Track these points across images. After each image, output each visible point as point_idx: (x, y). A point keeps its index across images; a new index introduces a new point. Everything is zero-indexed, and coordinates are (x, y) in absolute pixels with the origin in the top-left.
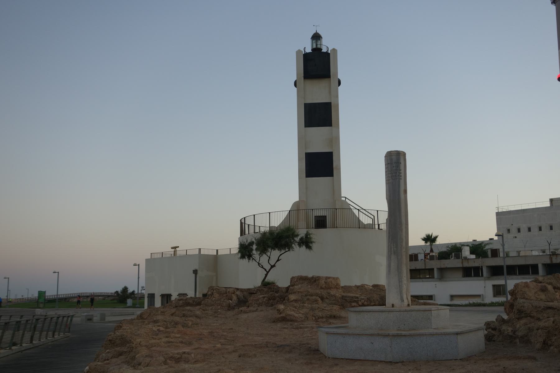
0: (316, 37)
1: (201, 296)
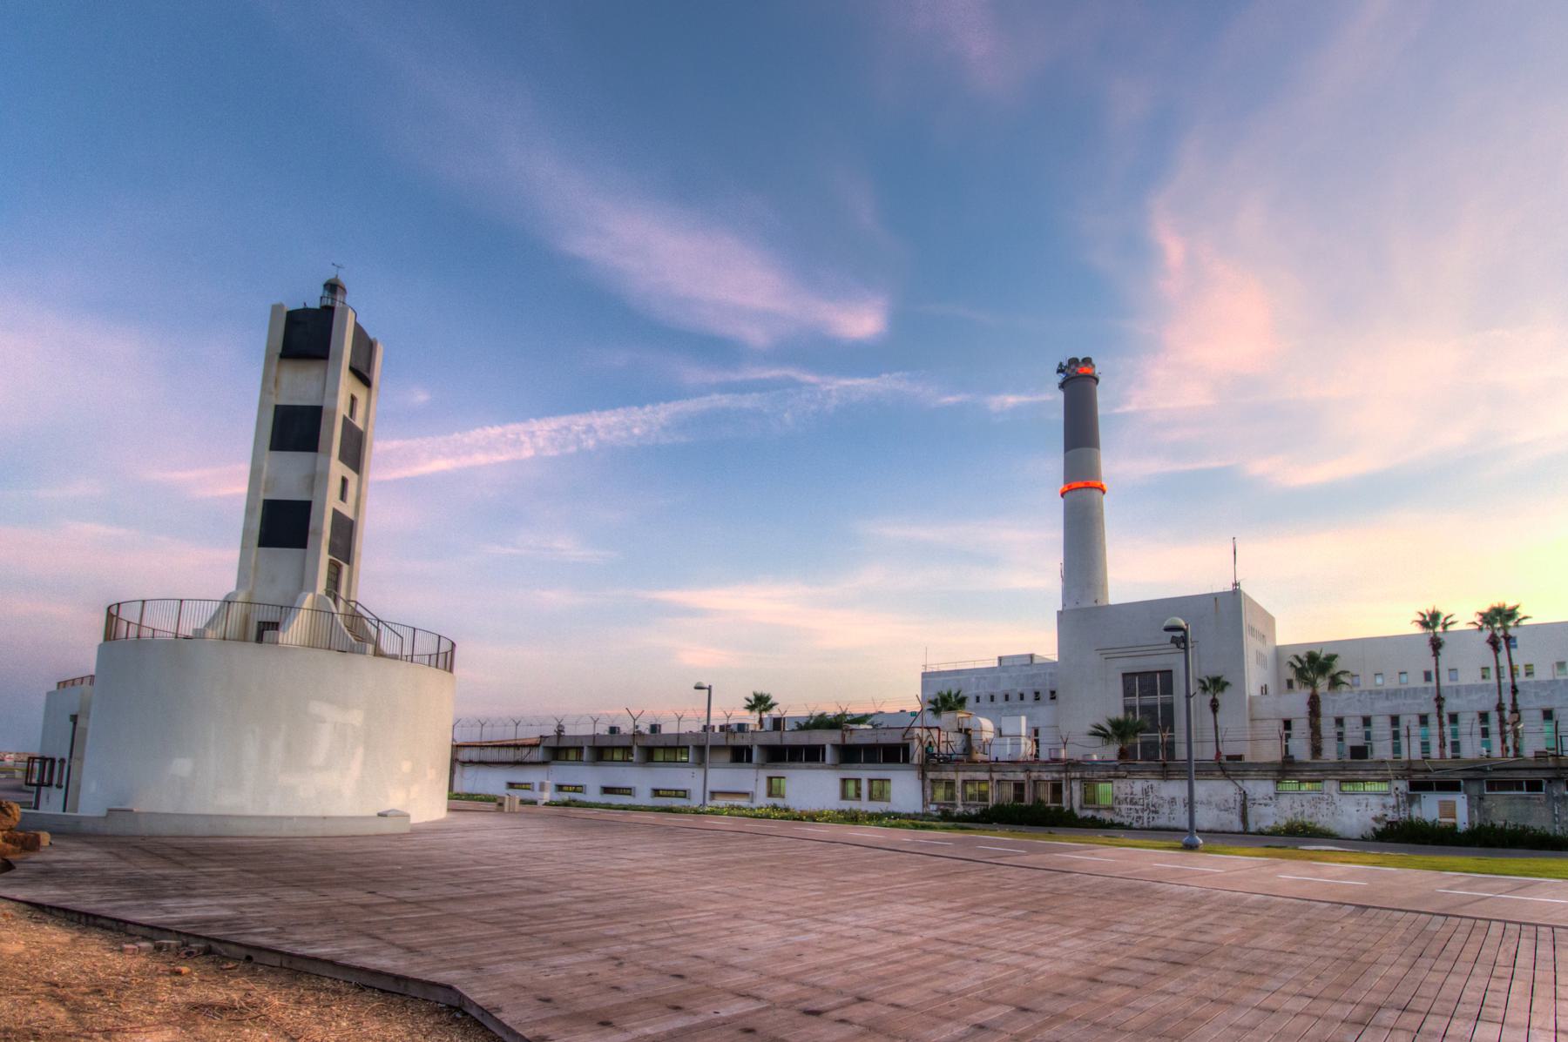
0: (333, 287)
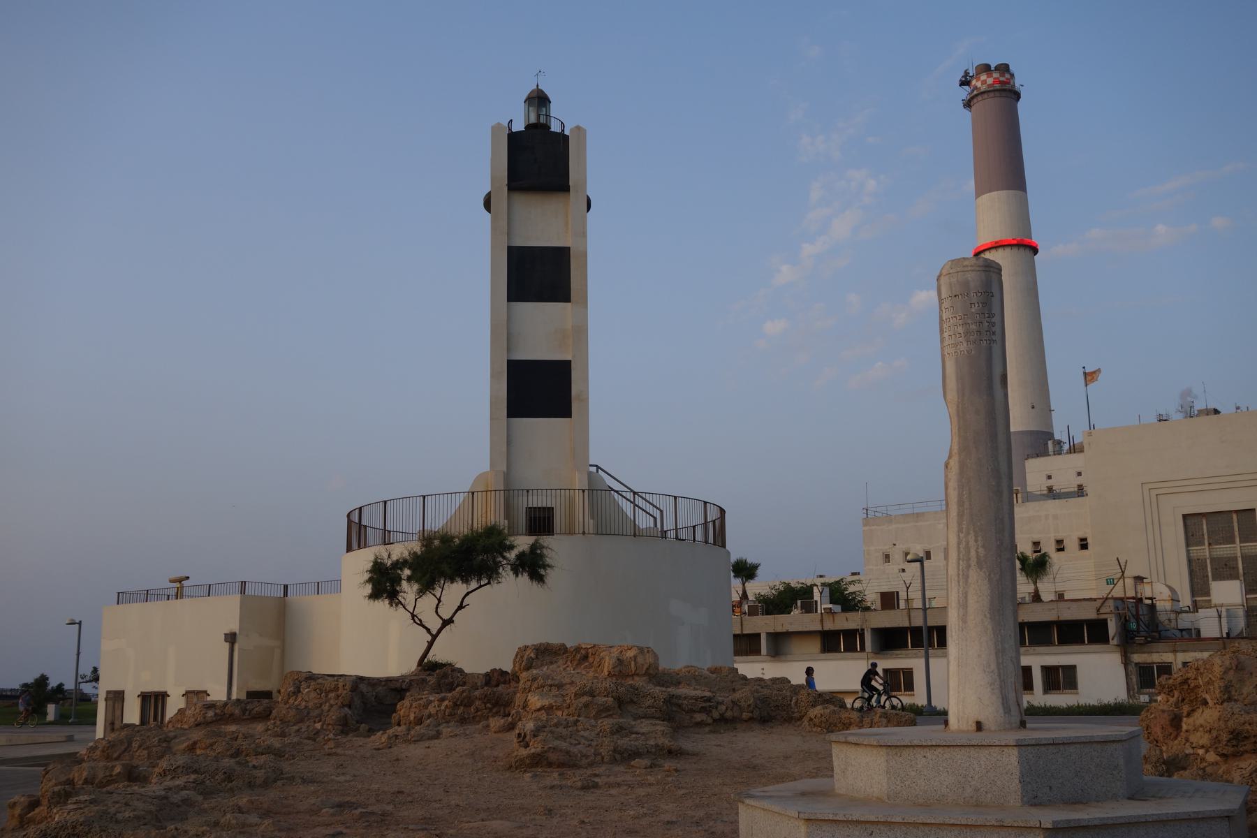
0: (539, 100)
1: (243, 697)
